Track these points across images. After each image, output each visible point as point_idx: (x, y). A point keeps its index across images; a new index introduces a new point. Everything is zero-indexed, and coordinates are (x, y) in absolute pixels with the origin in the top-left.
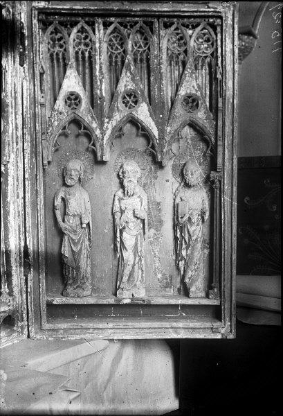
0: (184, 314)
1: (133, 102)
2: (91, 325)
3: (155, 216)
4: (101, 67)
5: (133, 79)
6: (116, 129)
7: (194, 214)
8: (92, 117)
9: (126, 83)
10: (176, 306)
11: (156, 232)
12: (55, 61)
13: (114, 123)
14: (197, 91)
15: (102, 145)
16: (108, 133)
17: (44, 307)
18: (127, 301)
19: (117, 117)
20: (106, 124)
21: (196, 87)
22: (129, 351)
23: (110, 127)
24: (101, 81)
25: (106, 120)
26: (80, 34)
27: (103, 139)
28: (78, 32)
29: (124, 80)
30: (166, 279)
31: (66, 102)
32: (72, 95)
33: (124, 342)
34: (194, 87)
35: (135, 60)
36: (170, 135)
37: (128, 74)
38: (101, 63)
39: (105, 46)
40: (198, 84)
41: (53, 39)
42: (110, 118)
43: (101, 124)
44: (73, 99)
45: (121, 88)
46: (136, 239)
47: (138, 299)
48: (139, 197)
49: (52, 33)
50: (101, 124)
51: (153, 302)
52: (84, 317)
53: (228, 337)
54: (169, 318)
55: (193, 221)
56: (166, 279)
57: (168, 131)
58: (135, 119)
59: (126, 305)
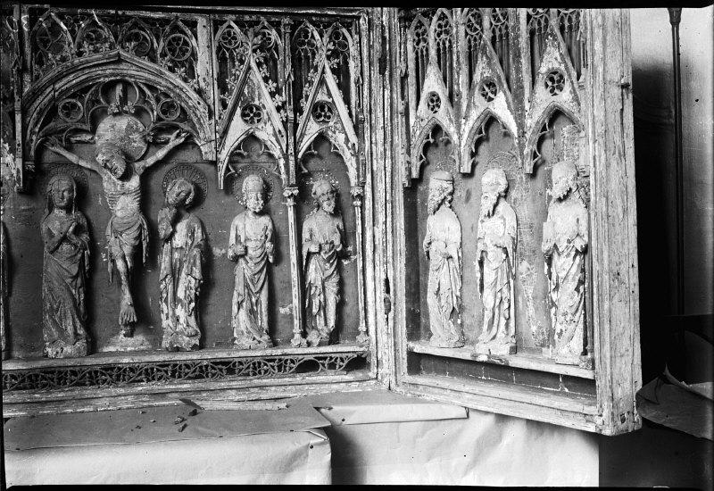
0: (567, 390)
1: (492, 92)
2: (467, 388)
3: (528, 244)
4: (458, 57)
5: (489, 64)
6: (473, 132)
7: (562, 239)
8: (450, 119)
9: (482, 71)
10: (556, 376)
11: (529, 266)
12: (589, 27)
13: (471, 123)
14: (560, 64)
15: (459, 154)
16: (465, 136)
17: (404, 355)
18: (483, 358)
19: (474, 114)
20: (463, 126)
21: (559, 58)
22: (515, 432)
23: (467, 130)
24: (458, 73)
25: (463, 121)
26: (440, 22)
27: (460, 146)
28: (439, 19)
29: (480, 68)
30: (543, 333)
31: (429, 105)
32: (434, 96)
33: (502, 418)
34: (556, 59)
35: (562, 29)
36: (531, 130)
37: (484, 58)
38: (458, 52)
39: (462, 29)
40: (561, 54)
41: (418, 35)
42: (466, 118)
43: (459, 127)
44: (434, 100)
45: (477, 78)
46: (497, 273)
47: (495, 357)
48: (502, 217)
49: (416, 28)
50: (459, 127)
51: (512, 364)
52: (456, 375)
53: (603, 432)
54: (548, 391)
55: (560, 250)
56: (543, 333)
57: (528, 125)
58: (678, 93)
59: (482, 363)
